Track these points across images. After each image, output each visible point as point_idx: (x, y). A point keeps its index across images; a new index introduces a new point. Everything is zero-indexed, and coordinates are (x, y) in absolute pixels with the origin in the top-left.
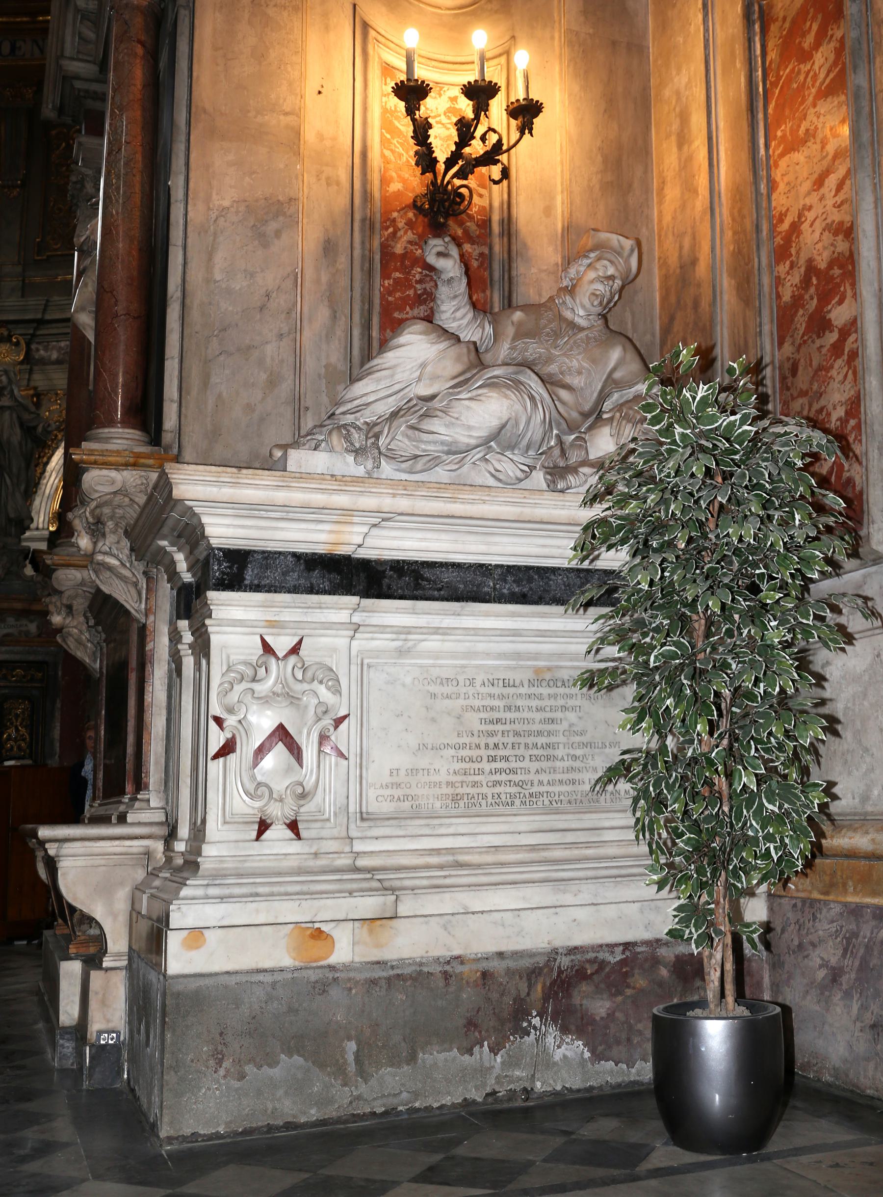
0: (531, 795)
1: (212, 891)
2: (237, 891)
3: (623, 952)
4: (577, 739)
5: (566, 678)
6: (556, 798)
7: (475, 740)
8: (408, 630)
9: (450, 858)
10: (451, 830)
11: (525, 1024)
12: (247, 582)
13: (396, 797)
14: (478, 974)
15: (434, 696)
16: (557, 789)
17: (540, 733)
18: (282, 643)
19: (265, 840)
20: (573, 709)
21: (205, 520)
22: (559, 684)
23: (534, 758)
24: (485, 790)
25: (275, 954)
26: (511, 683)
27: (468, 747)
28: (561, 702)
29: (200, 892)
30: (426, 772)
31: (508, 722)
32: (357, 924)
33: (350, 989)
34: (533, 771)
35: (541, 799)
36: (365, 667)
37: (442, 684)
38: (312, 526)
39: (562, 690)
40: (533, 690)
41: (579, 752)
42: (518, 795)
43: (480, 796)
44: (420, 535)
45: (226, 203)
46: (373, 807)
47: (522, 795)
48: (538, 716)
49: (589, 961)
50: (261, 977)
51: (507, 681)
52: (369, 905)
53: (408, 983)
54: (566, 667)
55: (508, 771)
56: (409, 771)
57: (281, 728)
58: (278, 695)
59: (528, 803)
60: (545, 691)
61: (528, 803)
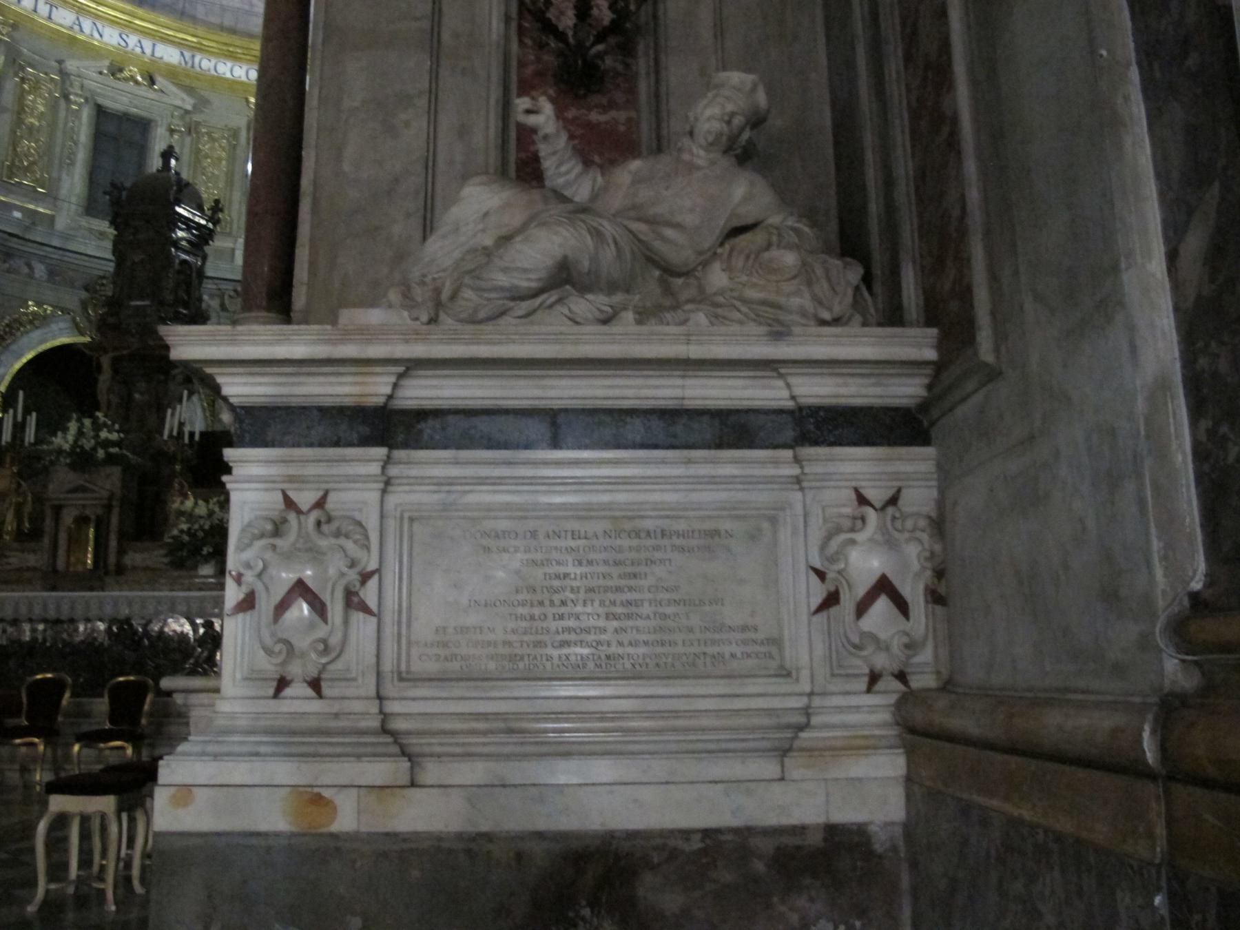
0: (608, 657)
1: (211, 748)
2: (236, 749)
3: (702, 840)
4: (666, 596)
7: (539, 597)
8: (451, 482)
9: (502, 725)
10: (505, 694)
11: (571, 914)
14: (511, 855)
15: (487, 550)
16: (642, 650)
17: (619, 589)
19: (285, 698)
20: (662, 561)
21: (220, 380)
22: (643, 535)
25: (272, 817)
26: (583, 534)
29: (197, 749)
32: (363, 791)
33: (354, 862)
34: (611, 630)
37: (497, 536)
41: (669, 610)
45: (356, 104)
46: (417, 667)
48: (615, 571)
49: (655, 848)
50: (254, 841)
52: (379, 771)
54: (651, 517)
60: (625, 542)
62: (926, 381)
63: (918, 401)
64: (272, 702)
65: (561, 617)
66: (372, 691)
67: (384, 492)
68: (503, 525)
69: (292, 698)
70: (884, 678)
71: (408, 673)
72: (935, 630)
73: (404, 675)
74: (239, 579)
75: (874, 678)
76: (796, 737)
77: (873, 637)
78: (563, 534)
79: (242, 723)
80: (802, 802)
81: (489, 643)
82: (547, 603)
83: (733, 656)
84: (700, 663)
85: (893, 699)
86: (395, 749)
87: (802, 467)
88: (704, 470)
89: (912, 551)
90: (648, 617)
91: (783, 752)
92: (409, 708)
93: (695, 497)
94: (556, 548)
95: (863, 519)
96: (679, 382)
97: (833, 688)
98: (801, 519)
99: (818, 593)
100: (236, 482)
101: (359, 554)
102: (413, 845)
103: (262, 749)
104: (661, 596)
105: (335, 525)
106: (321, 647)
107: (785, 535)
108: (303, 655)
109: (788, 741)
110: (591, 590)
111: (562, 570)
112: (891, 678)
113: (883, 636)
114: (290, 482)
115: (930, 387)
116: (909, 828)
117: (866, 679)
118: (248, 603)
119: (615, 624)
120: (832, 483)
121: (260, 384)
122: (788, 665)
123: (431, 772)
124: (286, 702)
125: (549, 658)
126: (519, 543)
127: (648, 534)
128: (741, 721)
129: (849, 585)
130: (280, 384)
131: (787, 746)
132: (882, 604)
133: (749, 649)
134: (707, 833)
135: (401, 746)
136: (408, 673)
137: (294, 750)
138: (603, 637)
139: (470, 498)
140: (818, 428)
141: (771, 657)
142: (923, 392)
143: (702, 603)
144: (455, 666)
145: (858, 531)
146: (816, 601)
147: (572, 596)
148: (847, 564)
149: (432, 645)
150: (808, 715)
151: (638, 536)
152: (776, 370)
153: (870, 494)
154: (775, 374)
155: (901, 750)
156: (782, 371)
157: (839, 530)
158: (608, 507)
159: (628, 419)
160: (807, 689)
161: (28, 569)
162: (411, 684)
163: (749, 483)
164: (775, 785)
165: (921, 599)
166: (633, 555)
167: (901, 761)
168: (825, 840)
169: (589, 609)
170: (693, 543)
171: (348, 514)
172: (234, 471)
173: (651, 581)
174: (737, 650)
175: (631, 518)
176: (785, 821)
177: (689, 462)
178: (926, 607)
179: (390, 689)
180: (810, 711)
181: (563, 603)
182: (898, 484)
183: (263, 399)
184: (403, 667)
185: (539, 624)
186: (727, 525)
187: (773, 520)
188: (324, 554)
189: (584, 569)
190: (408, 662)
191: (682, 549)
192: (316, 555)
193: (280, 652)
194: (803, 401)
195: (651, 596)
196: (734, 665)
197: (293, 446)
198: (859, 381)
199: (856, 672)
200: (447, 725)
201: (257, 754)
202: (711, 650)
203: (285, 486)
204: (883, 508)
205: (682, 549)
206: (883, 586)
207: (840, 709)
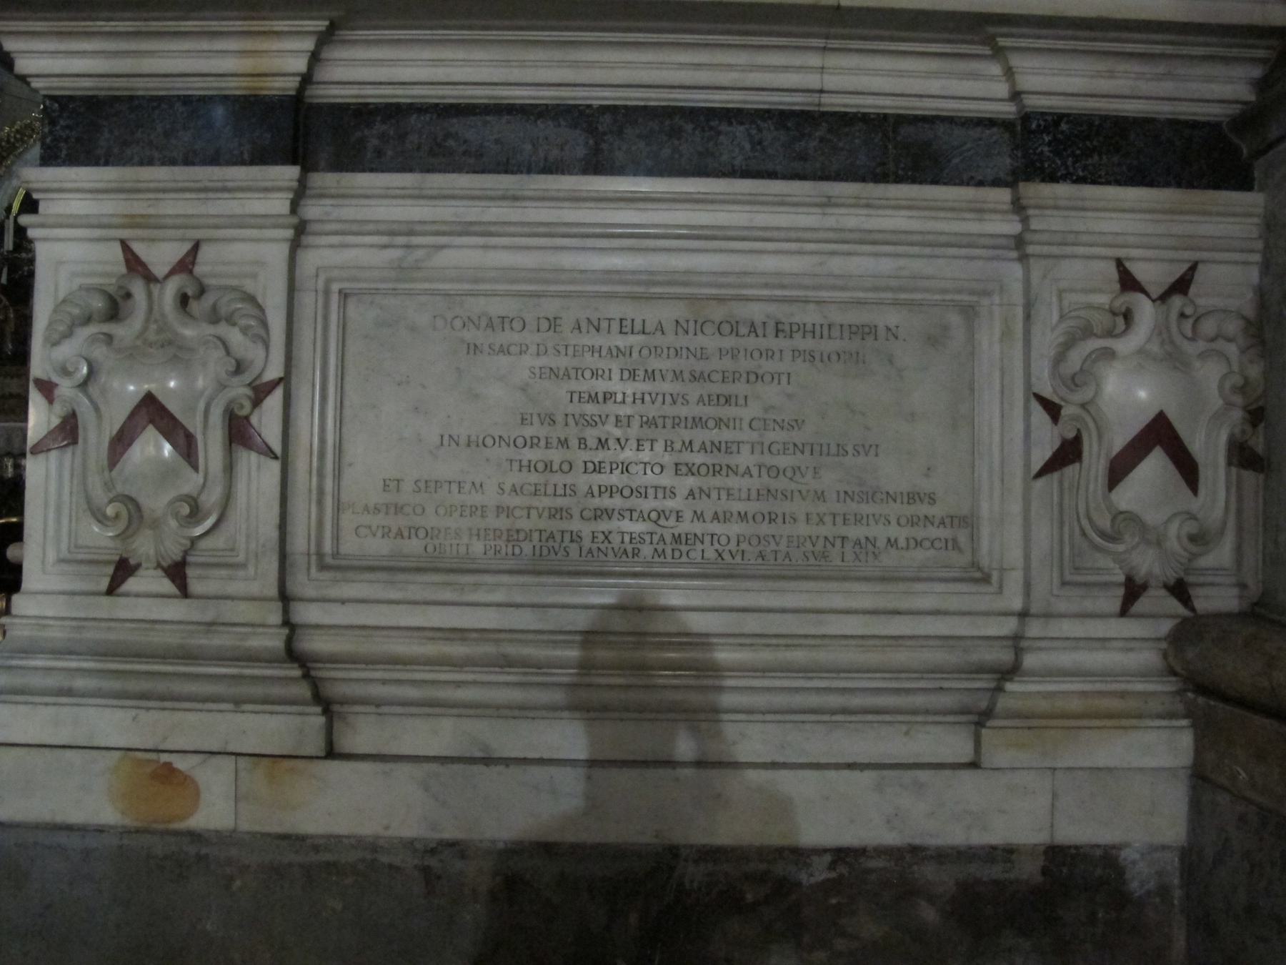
0: (677, 539)
2: (36, 681)
3: (832, 866)
5: (758, 319)
6: (732, 546)
7: (559, 432)
9: (489, 649)
12: (99, 152)
13: (394, 530)
15: (474, 349)
16: (735, 528)
17: (698, 422)
18: (161, 256)
19: (127, 595)
22: (743, 330)
23: (684, 469)
24: (575, 525)
25: (89, 800)
27: (543, 443)
28: (745, 364)
30: (455, 487)
31: (629, 400)
32: (243, 762)
33: (231, 879)
34: (682, 492)
35: (699, 546)
36: (335, 298)
37: (490, 325)
38: (205, 45)
39: (752, 342)
40: (683, 341)
41: (783, 461)
42: (647, 538)
43: (567, 537)
44: (427, 53)
46: (350, 545)
47: (656, 538)
48: (694, 391)
50: (62, 838)
51: (629, 323)
53: (349, 881)
55: (626, 492)
56: (422, 485)
57: (149, 401)
58: (151, 345)
59: (668, 552)
60: (710, 342)
61: (668, 552)
62: (1257, 72)
63: (1235, 109)
64: (106, 600)
65: (598, 469)
66: (273, 591)
67: (296, 245)
68: (497, 307)
69: (137, 595)
70: (1151, 592)
71: (336, 555)
72: (1239, 512)
73: (329, 560)
74: (47, 389)
75: (1133, 590)
76: (999, 689)
77: (1132, 518)
78: (604, 325)
79: (56, 634)
80: (1011, 807)
81: (474, 510)
82: (574, 443)
83: (892, 543)
84: (835, 553)
85: (1166, 627)
86: (304, 691)
87: (1025, 220)
88: (853, 220)
89: (1210, 374)
90: (748, 472)
91: (981, 718)
92: (332, 617)
93: (836, 265)
94: (592, 349)
95: (1128, 316)
96: (814, 60)
97: (1062, 606)
98: (1019, 311)
99: (1046, 441)
100: (42, 226)
101: (254, 353)
102: (327, 857)
103: (80, 683)
104: (771, 436)
105: (208, 300)
106: (186, 510)
107: (989, 341)
108: (156, 525)
109: (986, 696)
110: (650, 423)
111: (601, 386)
112: (1163, 592)
113: (1153, 517)
114: (131, 226)
115: (1262, 85)
116: (1189, 856)
117: (1121, 592)
118: (69, 430)
119: (691, 481)
120: (1081, 250)
121: (83, 54)
122: (985, 562)
123: (363, 734)
124: (122, 600)
125: (576, 538)
126: (530, 338)
127: (753, 328)
128: (901, 657)
129: (1098, 428)
130: (116, 54)
131: (983, 705)
132: (1155, 465)
133: (920, 533)
134: (841, 855)
135: (315, 685)
136: (336, 555)
137: (133, 685)
138: (670, 504)
139: (446, 258)
140: (1057, 153)
141: (956, 546)
142: (1248, 95)
143: (841, 450)
144: (414, 546)
145: (1117, 336)
146: (1042, 455)
147: (618, 432)
148: (1096, 394)
149: (377, 510)
150: (1019, 652)
151: (734, 331)
152: (990, 41)
153: (1140, 271)
154: (987, 51)
155: (1185, 722)
156: (1002, 42)
157: (1088, 332)
158: (686, 278)
159: (724, 127)
160: (1017, 604)
161: (11, 396)
162: (339, 575)
163: (930, 245)
164: (966, 775)
165: (1222, 461)
166: (727, 364)
167: (1186, 740)
168: (1045, 871)
169: (646, 456)
170: (828, 346)
171: (234, 282)
172: (41, 208)
173: (746, 414)
174: (901, 534)
175: (720, 300)
176: (979, 838)
177: (828, 203)
178: (1228, 474)
179: (301, 584)
180: (1024, 644)
181: (602, 444)
182: (1188, 255)
183: (87, 83)
184: (328, 547)
185: (559, 479)
186: (892, 318)
187: (969, 312)
188: (191, 350)
189: (641, 386)
190: (337, 538)
191: (811, 357)
192: (177, 354)
193: (117, 516)
194: (1033, 102)
195: (754, 436)
196: (889, 559)
197: (141, 164)
198: (1136, 67)
199: (1106, 578)
200: (401, 647)
201: (69, 692)
202: (854, 532)
203: (125, 234)
204: (1164, 297)
205: (811, 357)
206: (1159, 434)
207: (1076, 643)
